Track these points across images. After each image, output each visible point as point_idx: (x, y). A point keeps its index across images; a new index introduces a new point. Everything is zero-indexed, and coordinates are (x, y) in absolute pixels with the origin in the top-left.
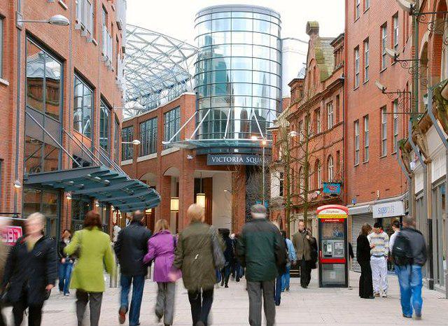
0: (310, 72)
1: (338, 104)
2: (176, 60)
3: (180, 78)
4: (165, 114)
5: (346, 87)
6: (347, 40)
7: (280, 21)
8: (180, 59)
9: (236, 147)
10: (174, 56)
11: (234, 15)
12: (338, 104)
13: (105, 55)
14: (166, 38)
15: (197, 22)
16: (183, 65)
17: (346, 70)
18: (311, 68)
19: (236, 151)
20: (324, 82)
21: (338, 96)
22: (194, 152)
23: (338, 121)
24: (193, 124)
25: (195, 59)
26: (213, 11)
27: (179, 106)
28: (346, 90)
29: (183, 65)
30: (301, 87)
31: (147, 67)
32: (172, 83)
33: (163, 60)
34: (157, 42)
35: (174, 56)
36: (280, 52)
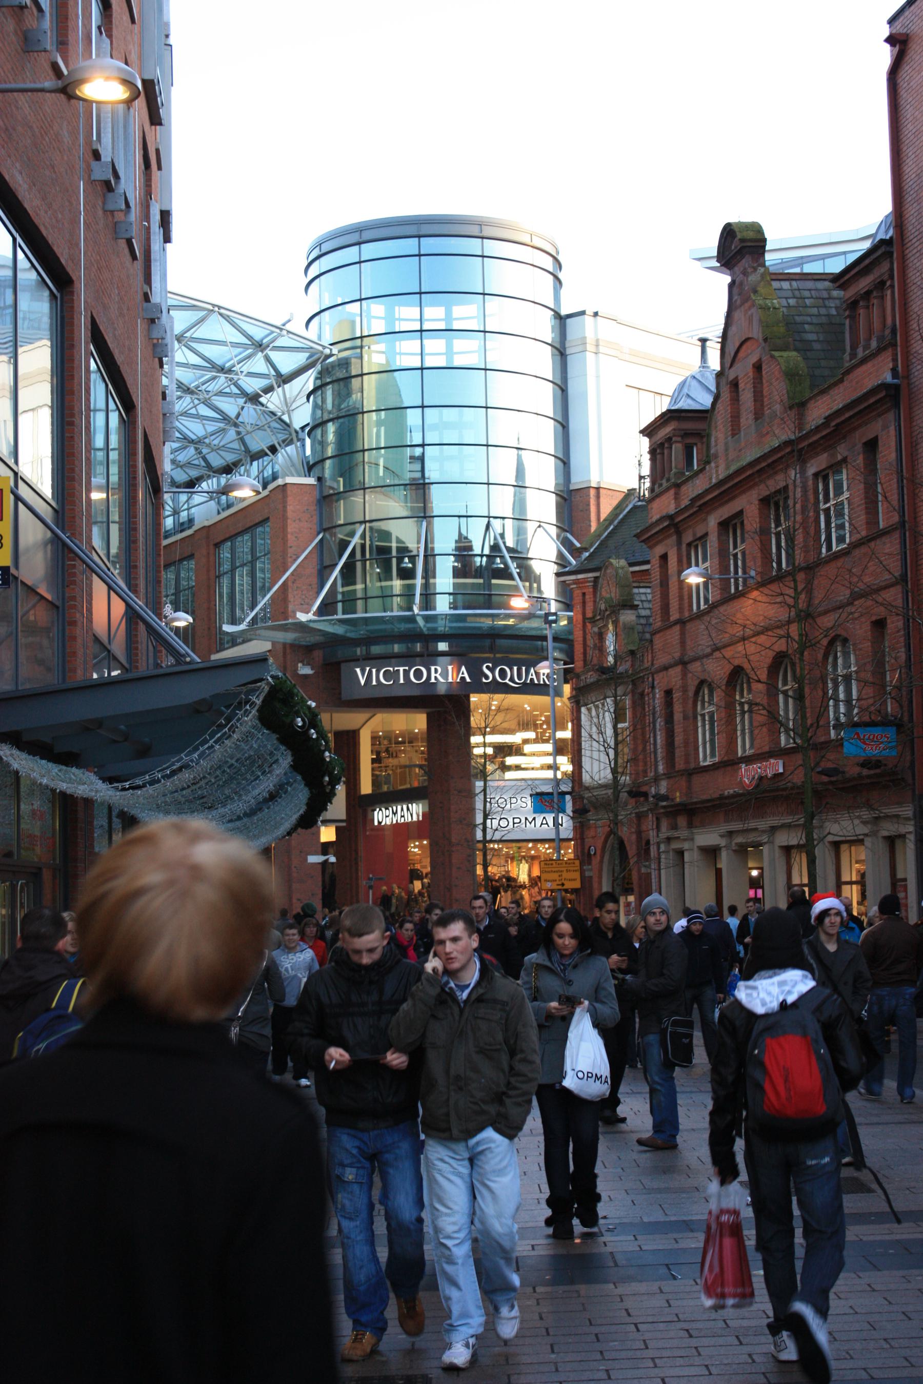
0: (735, 385)
1: (871, 467)
2: (253, 385)
3: (257, 443)
4: (217, 545)
5: (910, 409)
6: (903, 259)
7: (558, 264)
8: (264, 383)
9: (443, 637)
10: (250, 374)
11: (429, 245)
12: (871, 467)
13: (106, 157)
14: (227, 318)
15: (314, 271)
16: (273, 401)
17: (907, 354)
18: (744, 370)
19: (443, 646)
20: (799, 406)
21: (872, 446)
22: (318, 654)
23: (872, 519)
24: (312, 569)
25: (308, 381)
26: (365, 238)
27: (267, 519)
28: (910, 419)
29: (273, 401)
30: (702, 436)
31: (230, 371)
32: (230, 458)
33: (213, 387)
34: (199, 333)
35: (250, 374)
36: (561, 352)
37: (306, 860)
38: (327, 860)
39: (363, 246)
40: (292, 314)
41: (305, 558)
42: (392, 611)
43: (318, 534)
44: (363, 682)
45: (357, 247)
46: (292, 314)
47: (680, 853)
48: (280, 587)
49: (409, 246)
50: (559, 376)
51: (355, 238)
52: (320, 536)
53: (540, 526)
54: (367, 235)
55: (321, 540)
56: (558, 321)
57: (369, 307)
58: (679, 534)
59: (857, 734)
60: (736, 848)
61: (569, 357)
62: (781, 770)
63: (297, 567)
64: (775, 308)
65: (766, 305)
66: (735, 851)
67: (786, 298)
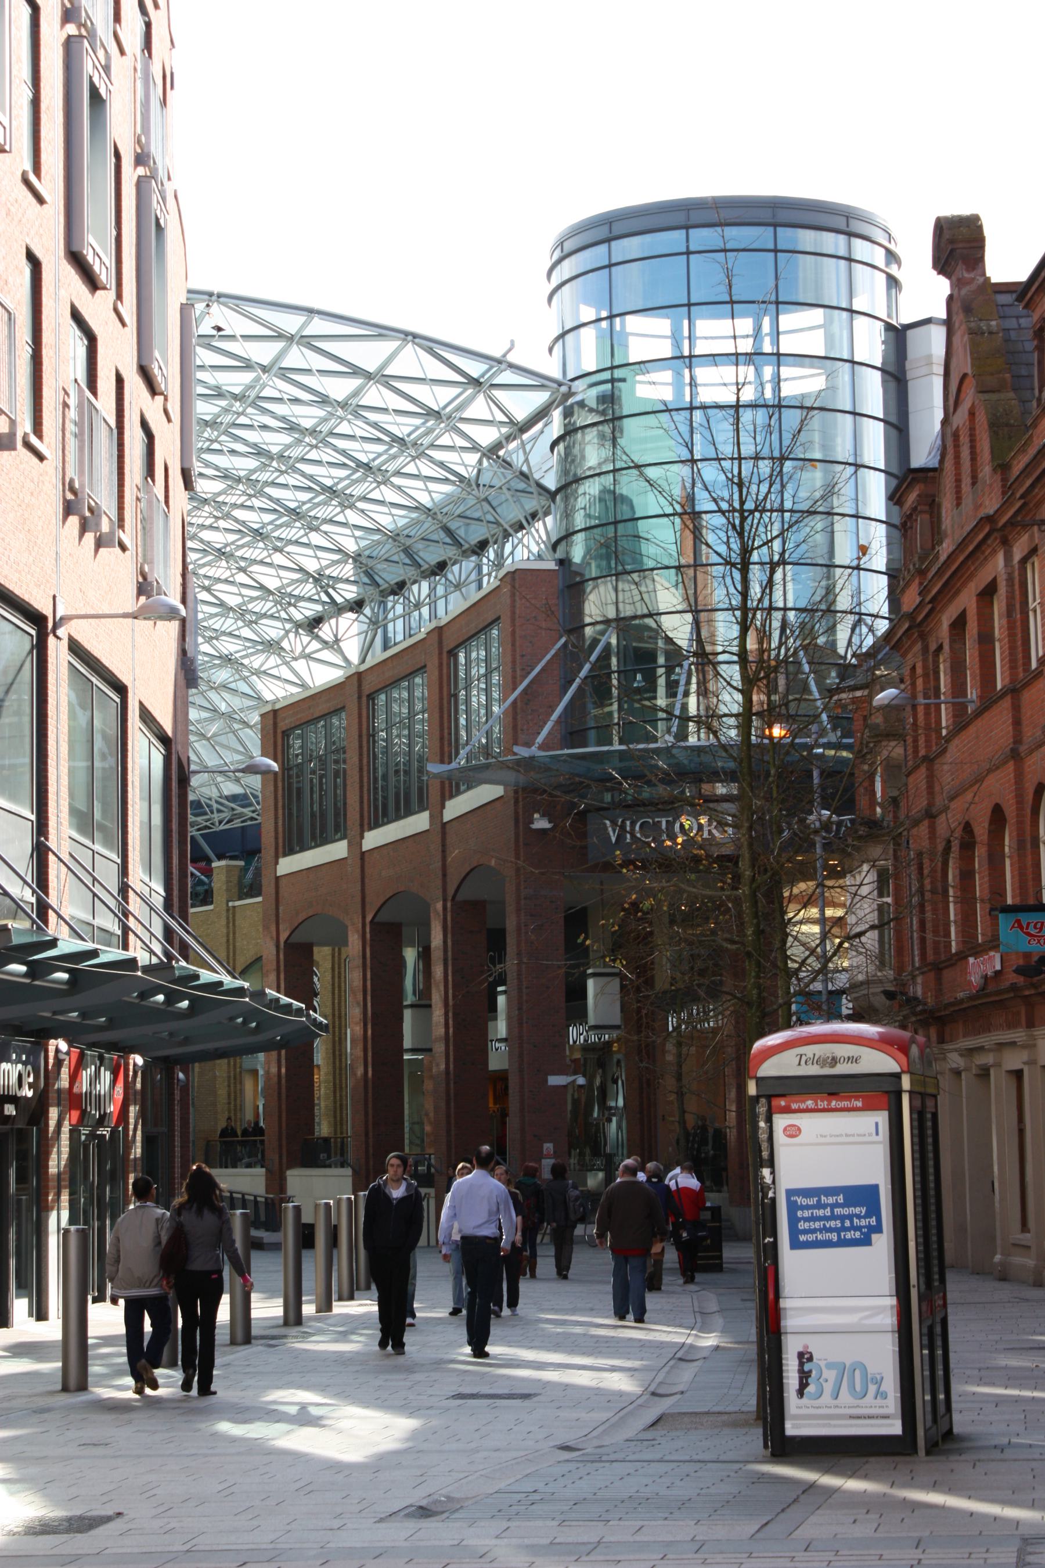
0: (956, 435)
37: (547, 1081)
38: (574, 1081)
39: (614, 244)
40: (512, 342)
41: (543, 670)
42: (611, 744)
43: (561, 637)
44: (613, 839)
45: (606, 245)
46: (512, 342)
47: (984, 1074)
48: (566, 708)
49: (674, 240)
50: (893, 409)
51: (680, 218)
52: (563, 640)
53: (859, 621)
54: (617, 229)
55: (565, 645)
56: (892, 334)
57: (623, 325)
58: (923, 637)
59: (1018, 921)
60: (979, 1072)
61: (910, 384)
62: (998, 967)
63: (532, 682)
64: (990, 333)
65: (980, 328)
66: (977, 1075)
67: (1017, 317)
